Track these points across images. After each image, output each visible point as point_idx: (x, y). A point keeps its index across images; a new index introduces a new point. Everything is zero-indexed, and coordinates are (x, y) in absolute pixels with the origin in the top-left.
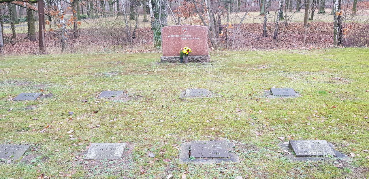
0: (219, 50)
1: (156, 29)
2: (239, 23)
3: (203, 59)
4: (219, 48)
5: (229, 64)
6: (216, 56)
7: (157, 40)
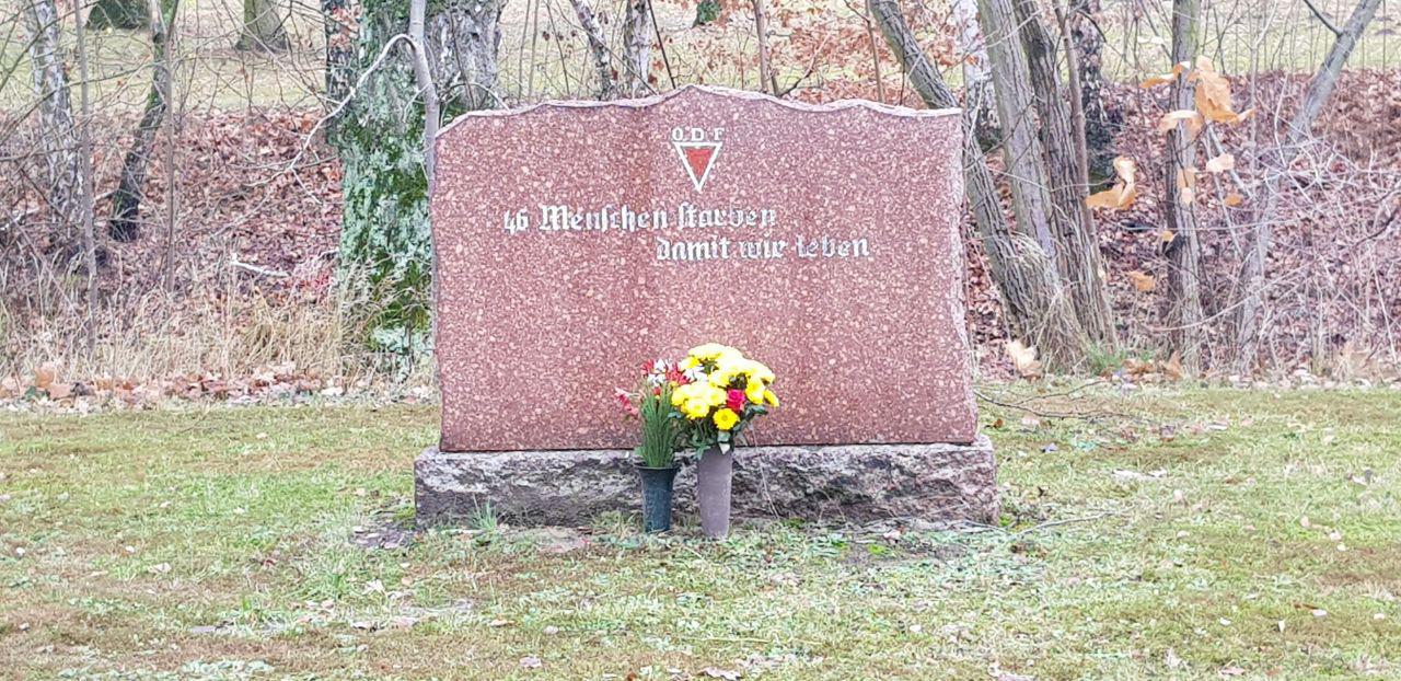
0: (1098, 370)
1: (369, 140)
2: (1304, 66)
3: (913, 485)
4: (1094, 349)
5: (1219, 550)
6: (1063, 445)
7: (383, 254)
